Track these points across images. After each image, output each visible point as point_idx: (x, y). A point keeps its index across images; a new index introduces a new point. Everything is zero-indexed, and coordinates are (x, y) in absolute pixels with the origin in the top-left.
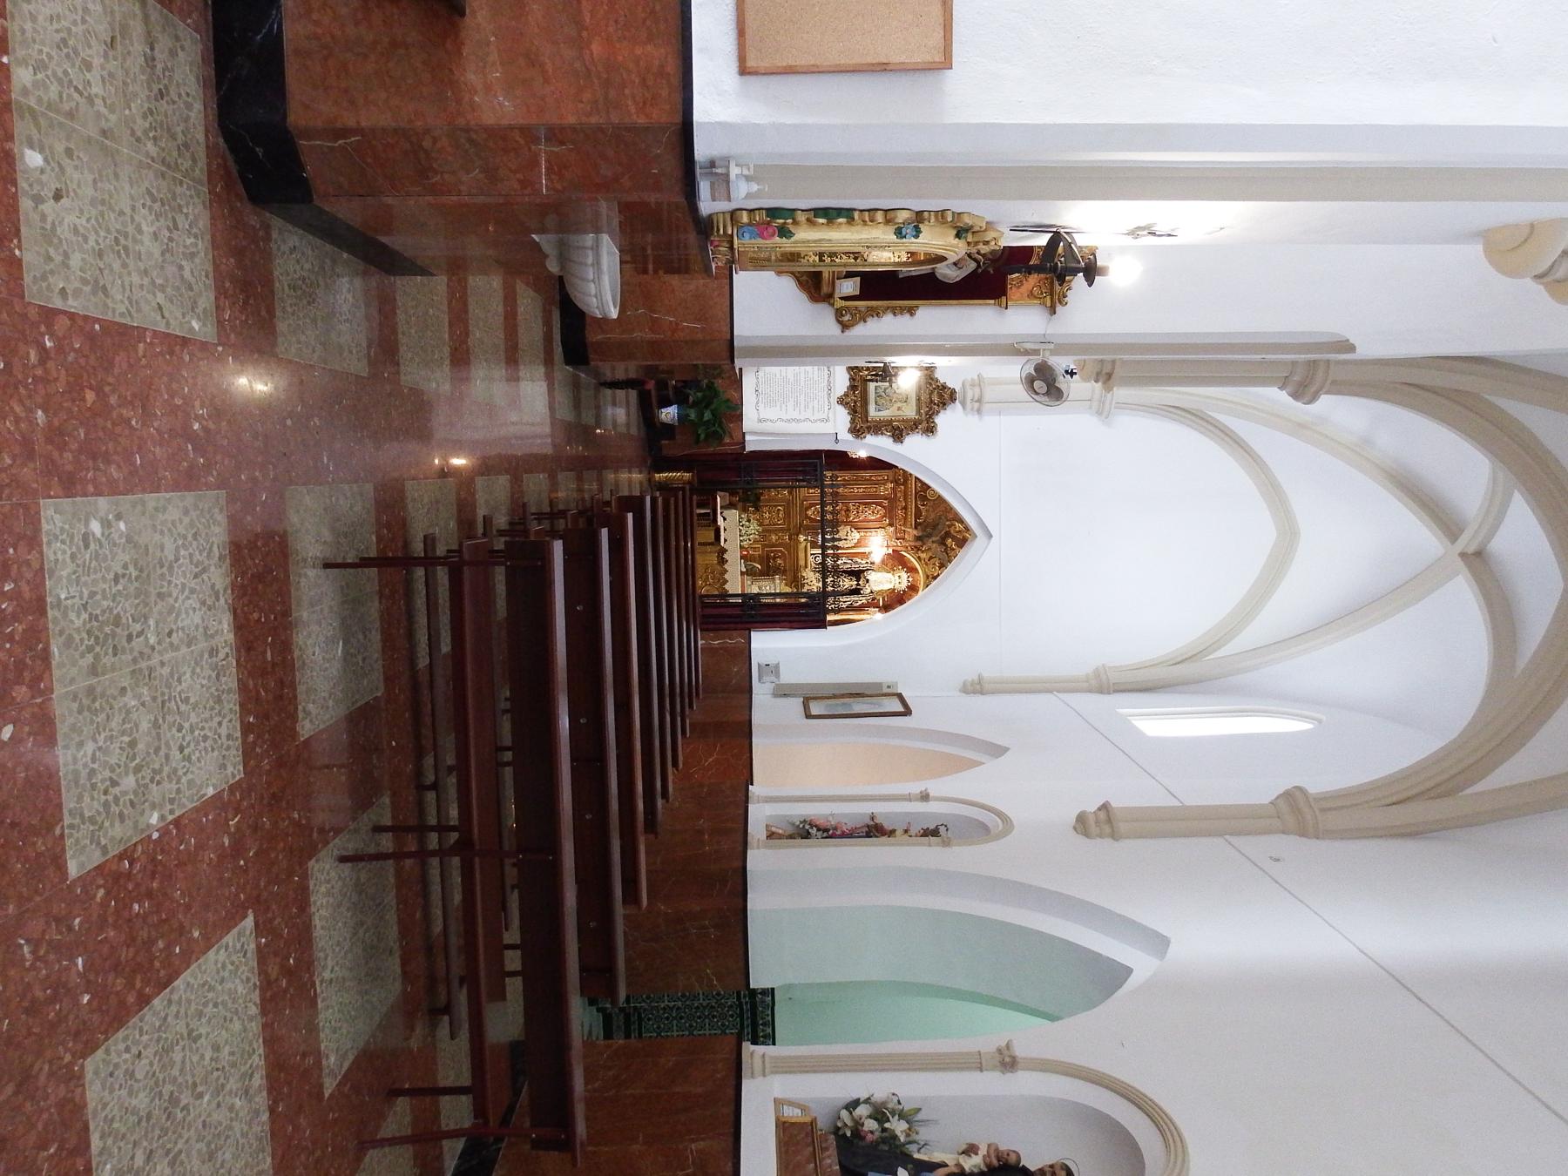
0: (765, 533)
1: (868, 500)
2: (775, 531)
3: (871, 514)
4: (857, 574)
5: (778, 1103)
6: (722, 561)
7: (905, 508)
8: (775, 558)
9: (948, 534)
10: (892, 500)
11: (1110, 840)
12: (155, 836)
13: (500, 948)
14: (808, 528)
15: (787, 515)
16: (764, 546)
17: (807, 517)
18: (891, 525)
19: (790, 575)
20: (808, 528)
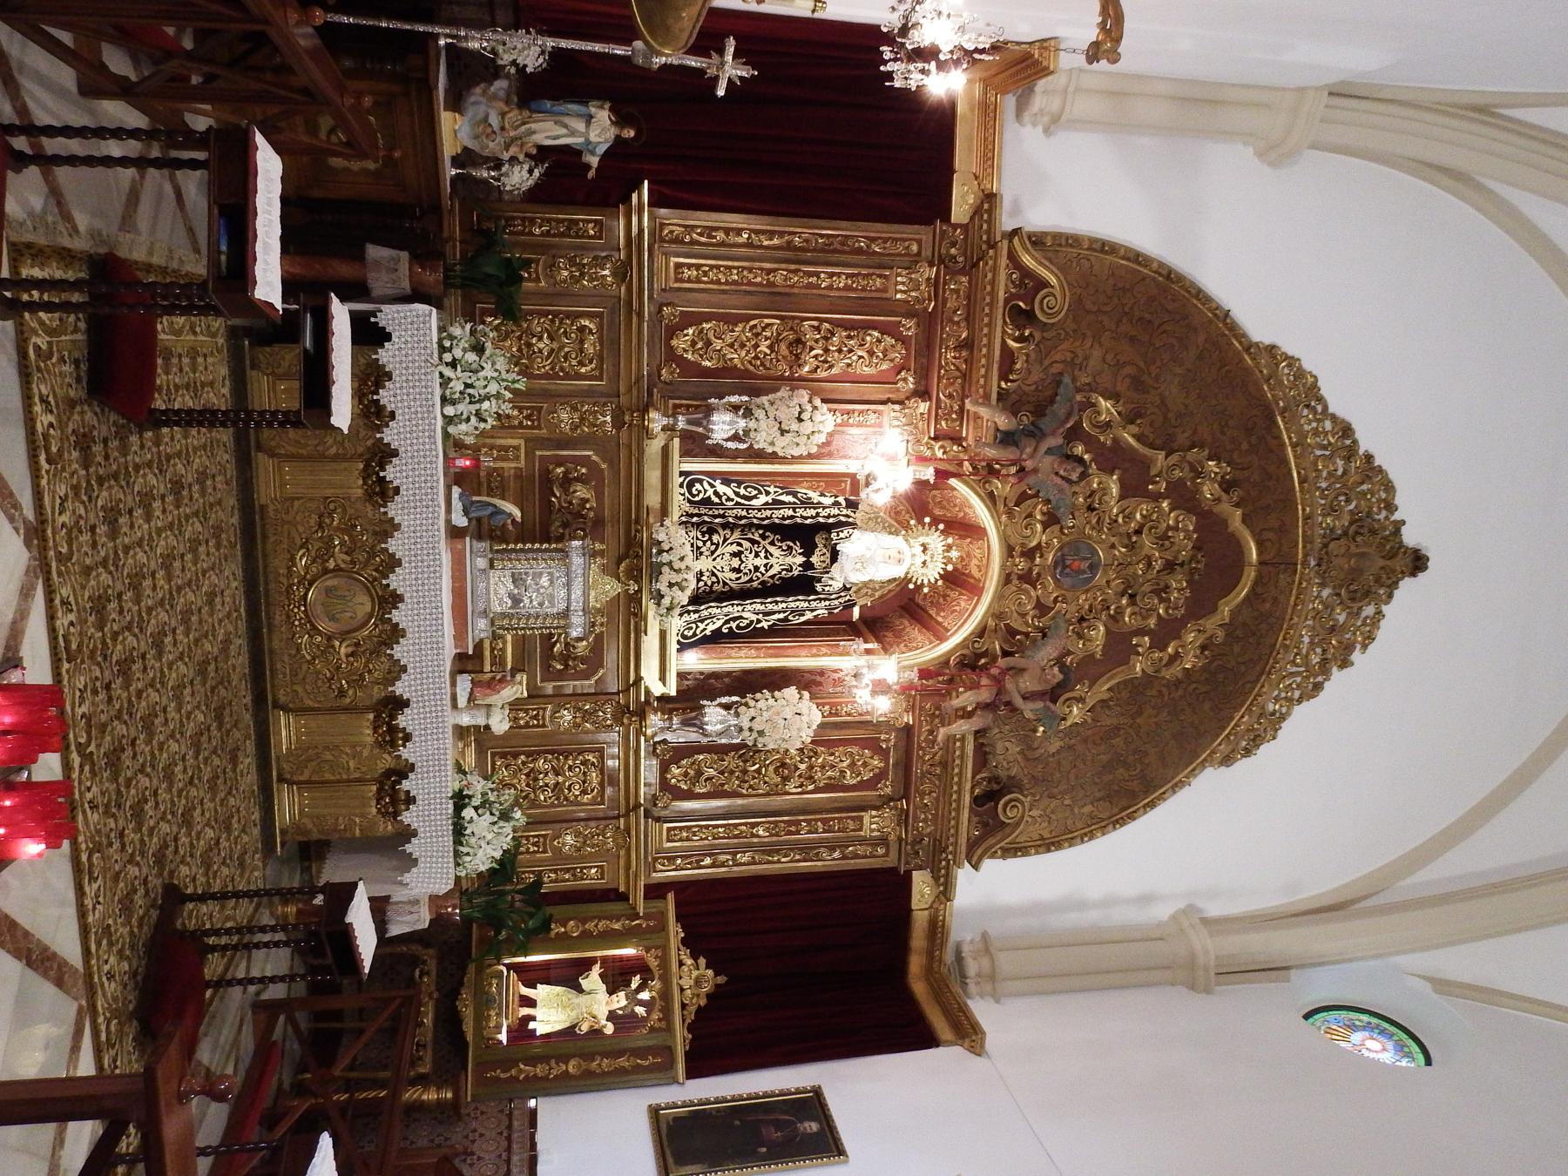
0: (534, 401)
1: (865, 313)
2: (565, 397)
3: (865, 358)
4: (805, 535)
5: (1205, 525)
6: (383, 492)
7: (968, 345)
8: (566, 482)
9: (1075, 434)
10: (929, 323)
11: (1184, 990)
12: (911, 586)
13: (610, 918)
14: (670, 390)
15: (611, 344)
16: (533, 443)
17: (672, 357)
18: (922, 393)
19: (609, 543)
20: (670, 390)
